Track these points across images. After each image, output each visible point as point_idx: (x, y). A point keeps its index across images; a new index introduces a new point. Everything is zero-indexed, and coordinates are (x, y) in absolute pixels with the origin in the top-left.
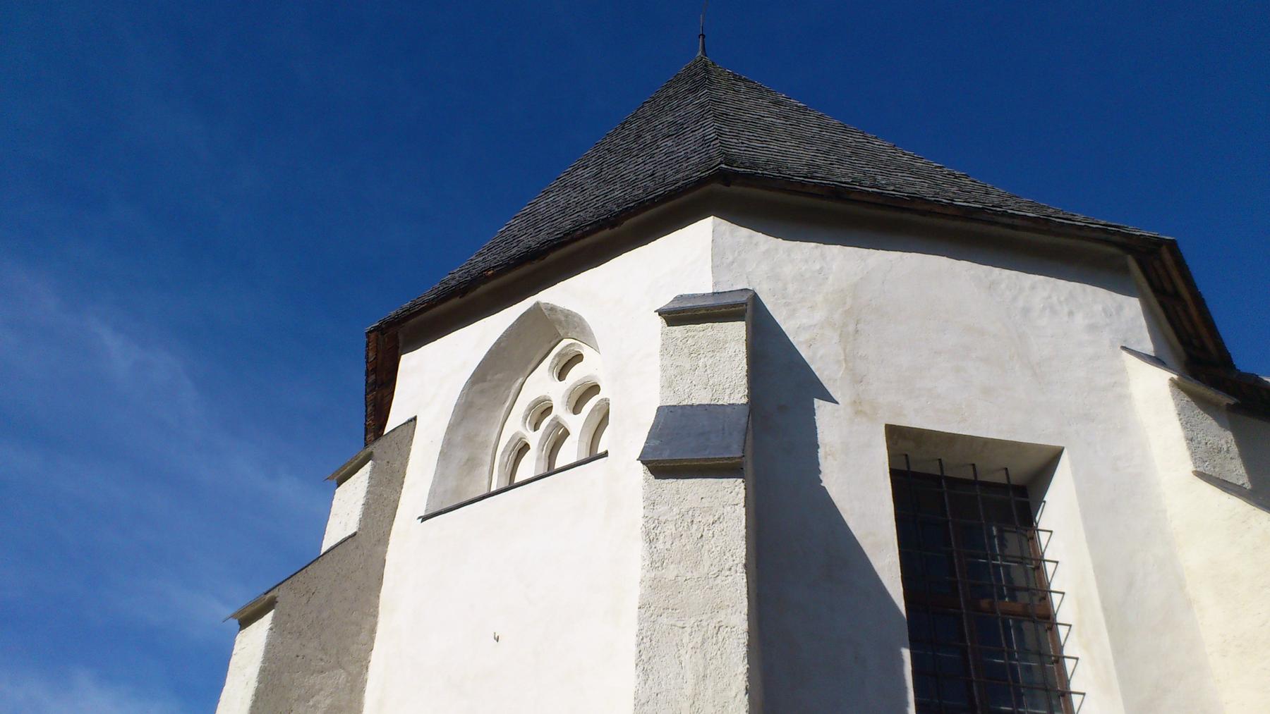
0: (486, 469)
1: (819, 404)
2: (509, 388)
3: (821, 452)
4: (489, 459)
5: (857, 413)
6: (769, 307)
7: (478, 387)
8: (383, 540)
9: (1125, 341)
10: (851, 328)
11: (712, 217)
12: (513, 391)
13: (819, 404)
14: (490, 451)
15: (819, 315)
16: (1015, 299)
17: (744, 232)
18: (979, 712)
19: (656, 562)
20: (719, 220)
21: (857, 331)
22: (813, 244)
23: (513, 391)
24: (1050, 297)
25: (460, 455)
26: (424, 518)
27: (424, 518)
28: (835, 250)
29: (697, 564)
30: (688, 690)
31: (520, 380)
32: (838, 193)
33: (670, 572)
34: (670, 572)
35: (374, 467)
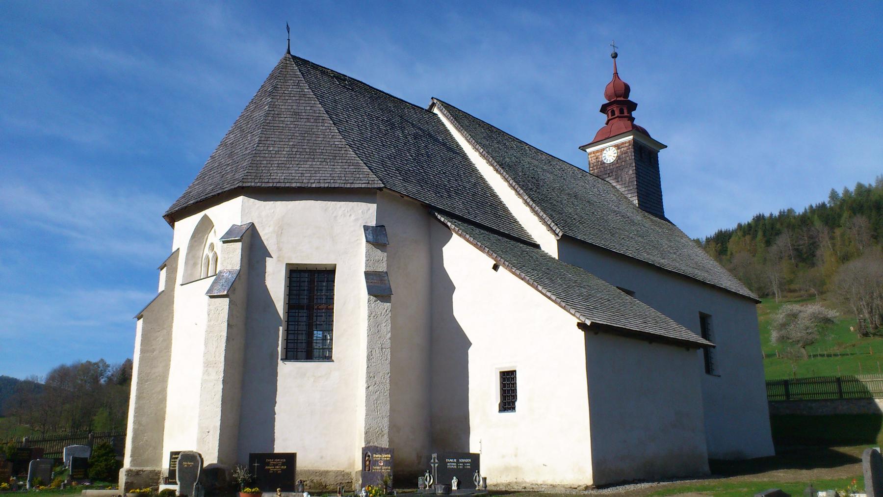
0: (200, 265)
1: (268, 259)
2: (204, 238)
3: (267, 274)
4: (200, 262)
5: (279, 261)
6: (257, 228)
7: (194, 240)
8: (173, 290)
9: (366, 223)
10: (280, 232)
11: (242, 197)
12: (205, 239)
13: (268, 259)
14: (201, 259)
15: (271, 229)
16: (333, 213)
17: (252, 200)
18: (1, 470)
19: (210, 321)
20: (244, 197)
21: (281, 233)
22: (272, 202)
23: (205, 239)
24: (345, 210)
25: (191, 262)
26: (182, 285)
27: (182, 285)
28: (279, 204)
29: (218, 320)
30: (214, 350)
31: (207, 235)
32: (278, 188)
33: (212, 323)
34: (212, 323)
35: (167, 269)
